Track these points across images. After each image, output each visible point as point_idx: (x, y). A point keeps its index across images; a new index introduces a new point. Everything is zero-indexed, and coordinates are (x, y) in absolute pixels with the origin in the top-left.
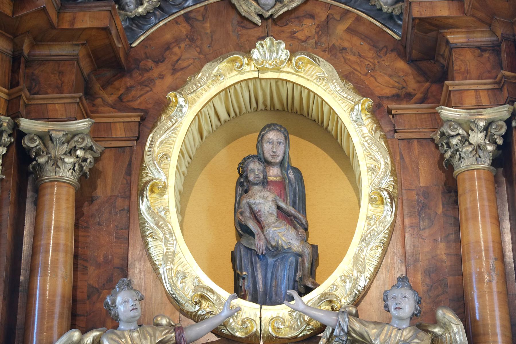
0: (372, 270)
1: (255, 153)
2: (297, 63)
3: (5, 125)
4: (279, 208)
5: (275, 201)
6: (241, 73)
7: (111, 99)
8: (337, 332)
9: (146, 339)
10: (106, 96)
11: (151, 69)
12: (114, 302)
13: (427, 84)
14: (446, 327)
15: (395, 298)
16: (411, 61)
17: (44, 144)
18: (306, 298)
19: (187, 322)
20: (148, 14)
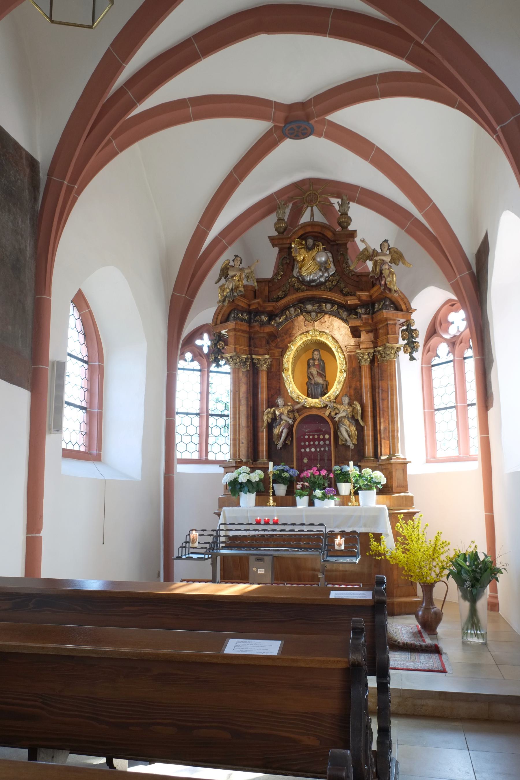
4: (318, 372)
7: (274, 345)
10: (273, 344)
11: (284, 336)
12: (278, 401)
14: (356, 405)
18: (323, 398)
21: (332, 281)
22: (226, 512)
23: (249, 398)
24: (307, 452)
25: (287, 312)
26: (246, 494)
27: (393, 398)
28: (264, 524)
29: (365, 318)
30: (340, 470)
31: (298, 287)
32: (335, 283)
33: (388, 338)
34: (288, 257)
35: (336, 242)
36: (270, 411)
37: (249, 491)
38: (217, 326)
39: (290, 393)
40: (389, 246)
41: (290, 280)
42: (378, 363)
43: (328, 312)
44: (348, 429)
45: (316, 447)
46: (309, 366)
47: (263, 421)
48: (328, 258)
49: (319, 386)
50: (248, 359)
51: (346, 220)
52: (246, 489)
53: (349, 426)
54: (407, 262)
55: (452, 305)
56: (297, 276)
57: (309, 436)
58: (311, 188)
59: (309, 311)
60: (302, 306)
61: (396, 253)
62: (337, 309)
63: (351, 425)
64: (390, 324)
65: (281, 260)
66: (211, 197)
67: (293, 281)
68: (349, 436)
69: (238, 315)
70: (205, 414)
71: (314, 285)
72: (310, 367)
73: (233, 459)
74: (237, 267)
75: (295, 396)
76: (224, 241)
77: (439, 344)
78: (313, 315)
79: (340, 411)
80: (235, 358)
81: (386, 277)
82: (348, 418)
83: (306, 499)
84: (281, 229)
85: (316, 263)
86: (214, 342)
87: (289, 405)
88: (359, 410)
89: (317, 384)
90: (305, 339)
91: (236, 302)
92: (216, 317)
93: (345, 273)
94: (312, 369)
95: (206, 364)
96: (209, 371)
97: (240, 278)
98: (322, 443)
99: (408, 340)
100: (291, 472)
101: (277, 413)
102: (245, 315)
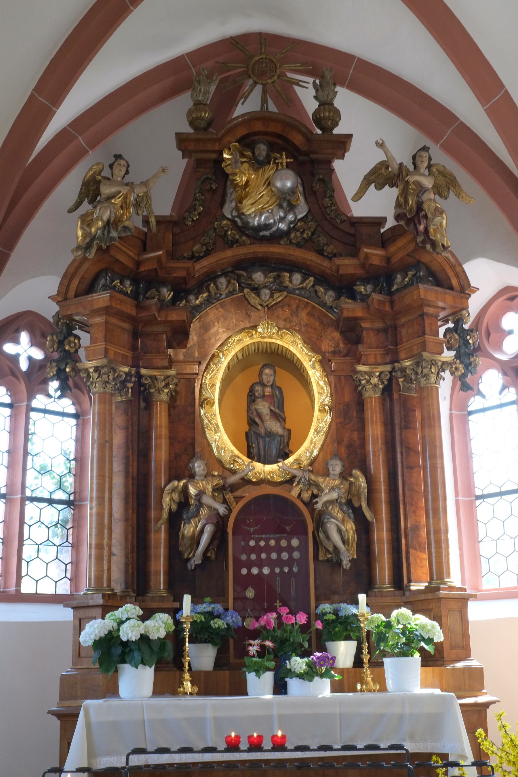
0: (320, 446)
1: (258, 381)
2: (281, 334)
3: (133, 372)
4: (271, 410)
5: (269, 407)
6: (252, 339)
8: (303, 480)
9: (209, 484)
12: (194, 466)
13: (350, 345)
14: (357, 478)
15: (332, 465)
16: (342, 333)
17: (152, 381)
18: (286, 462)
19: (227, 473)
20: (201, 303)
21: (301, 230)
22: (91, 711)
23: (131, 459)
24: (253, 575)
25: (212, 285)
26: (137, 667)
27: (437, 464)
28: (250, 750)
29: (379, 301)
30: (333, 614)
31: (233, 238)
32: (308, 234)
33: (425, 341)
34: (213, 178)
35: (311, 156)
36: (178, 486)
37: (143, 662)
38: (68, 302)
39: (215, 450)
40: (430, 159)
41: (216, 223)
42: (400, 394)
43: (294, 289)
44: (343, 528)
45: (271, 564)
46: (252, 398)
47: (162, 508)
48: (297, 186)
49: (273, 439)
50: (131, 376)
51: (331, 114)
52: (137, 656)
53: (343, 522)
54: (465, 193)
55: (512, 299)
56: (231, 215)
57: (258, 541)
58: (264, 49)
59: (256, 286)
60: (243, 275)
61: (442, 176)
62: (313, 286)
63: (346, 519)
64: (427, 314)
65: (200, 183)
66: (80, 19)
67: (222, 225)
68: (344, 542)
69: (114, 281)
70: (19, 496)
71: (267, 236)
72: (254, 401)
73: (97, 590)
74: (119, 179)
75: (226, 457)
76: (80, 138)
77: (484, 372)
78: (265, 294)
79: (323, 491)
80: (106, 370)
81: (429, 215)
82: (340, 504)
83: (268, 677)
84: (203, 122)
85: (272, 191)
86: (57, 337)
87: (214, 476)
88: (364, 488)
89: (270, 434)
90: (248, 341)
91: (113, 253)
92: (66, 282)
93: (328, 217)
94: (261, 404)
95: (24, 394)
96: (30, 409)
97: (126, 202)
98: (285, 556)
99: (458, 351)
100: (228, 618)
101: (192, 491)
102: (128, 283)
